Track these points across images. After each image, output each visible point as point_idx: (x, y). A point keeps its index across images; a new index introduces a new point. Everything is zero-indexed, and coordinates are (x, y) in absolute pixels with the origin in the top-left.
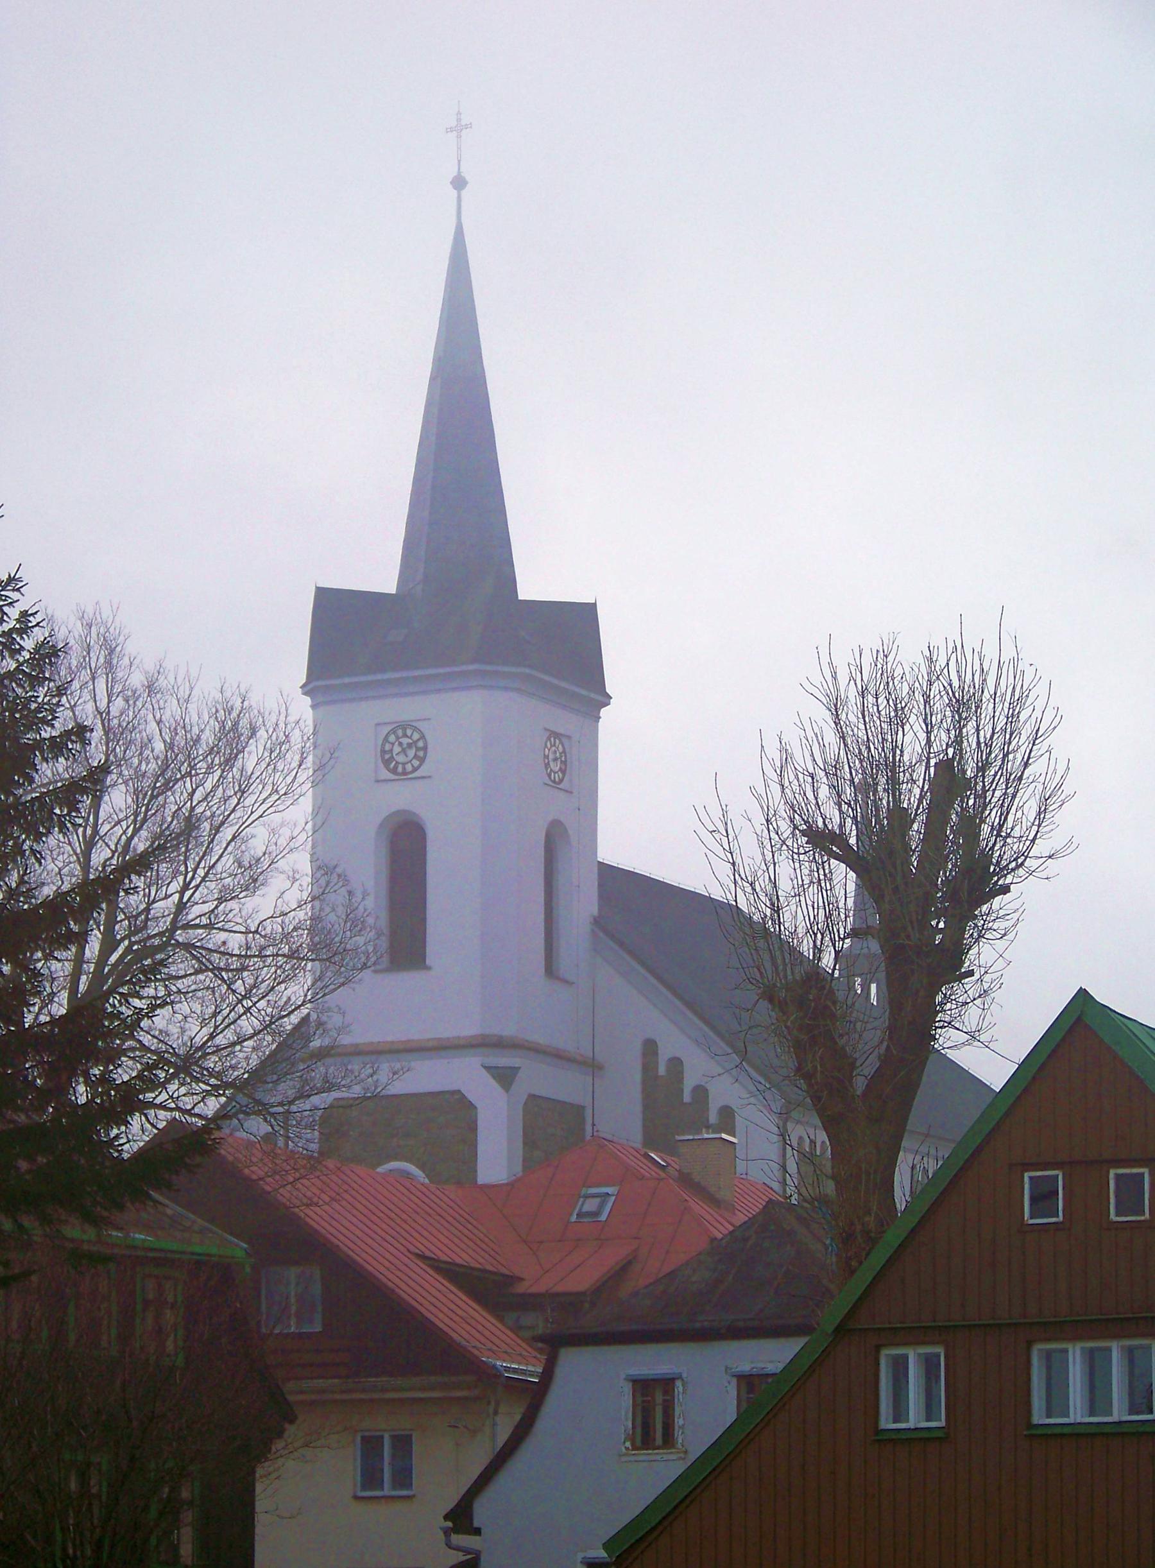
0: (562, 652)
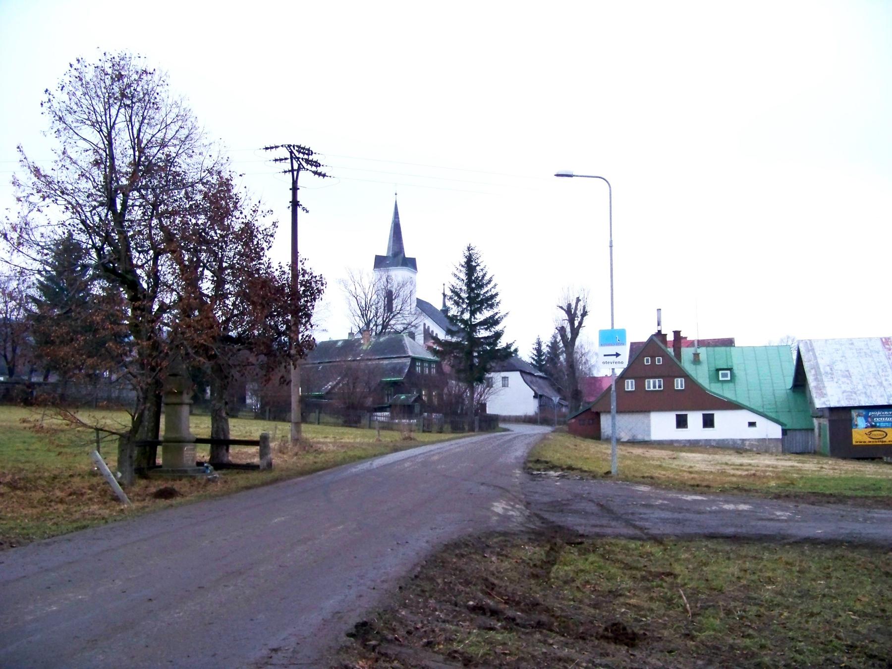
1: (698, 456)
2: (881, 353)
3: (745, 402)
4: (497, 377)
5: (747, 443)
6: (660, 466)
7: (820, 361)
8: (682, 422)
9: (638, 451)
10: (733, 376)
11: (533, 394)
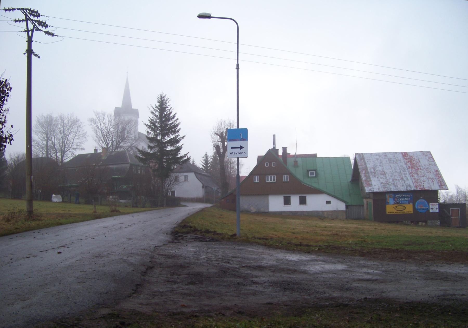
1: (298, 221)
2: (402, 161)
3: (324, 190)
4: (181, 177)
5: (326, 213)
6: (273, 228)
7: (368, 165)
8: (287, 201)
9: (260, 218)
10: (317, 174)
11: (201, 185)
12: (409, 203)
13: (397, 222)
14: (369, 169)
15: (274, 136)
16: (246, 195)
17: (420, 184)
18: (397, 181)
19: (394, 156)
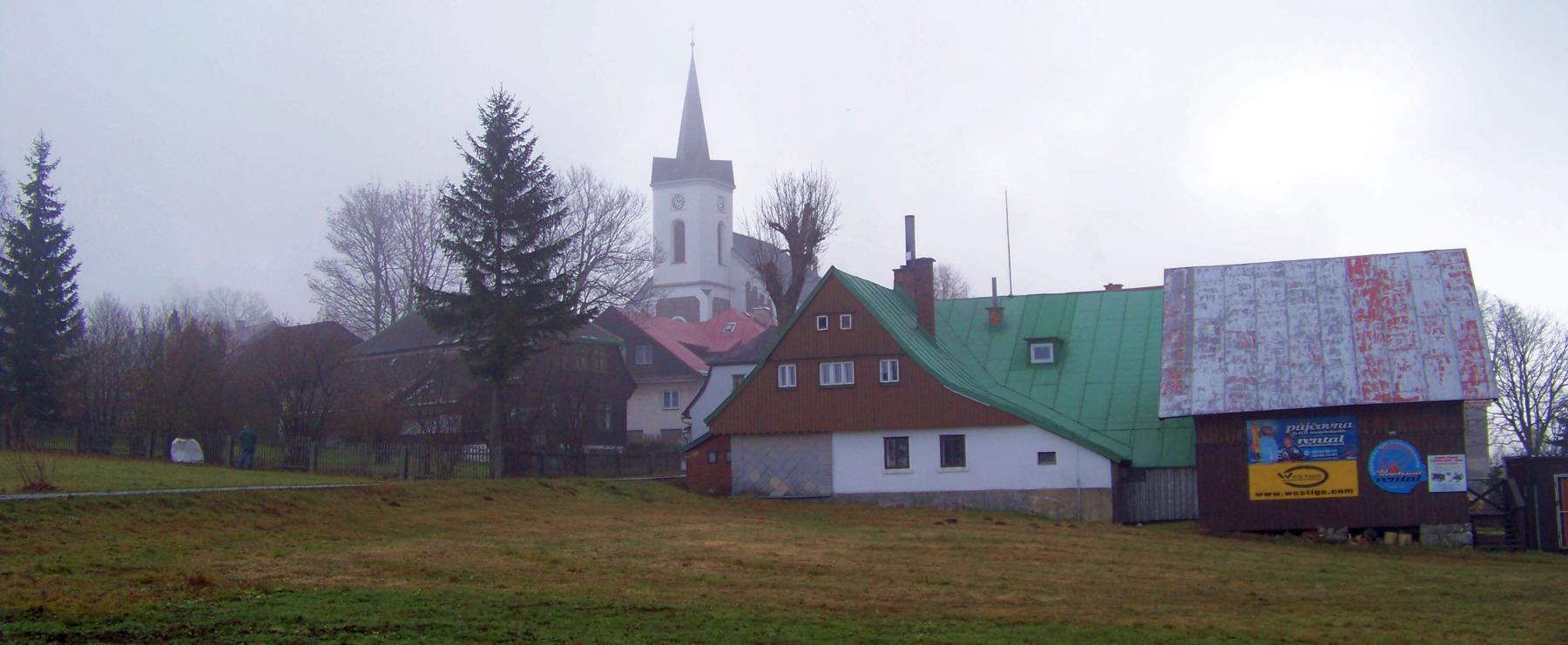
0: (722, 175)
2: (1339, 293)
5: (1036, 498)
7: (1199, 313)
8: (897, 455)
12: (1341, 456)
13: (1298, 532)
14: (1197, 325)
15: (910, 220)
16: (761, 435)
17: (1386, 378)
18: (1295, 371)
19: (1313, 274)
